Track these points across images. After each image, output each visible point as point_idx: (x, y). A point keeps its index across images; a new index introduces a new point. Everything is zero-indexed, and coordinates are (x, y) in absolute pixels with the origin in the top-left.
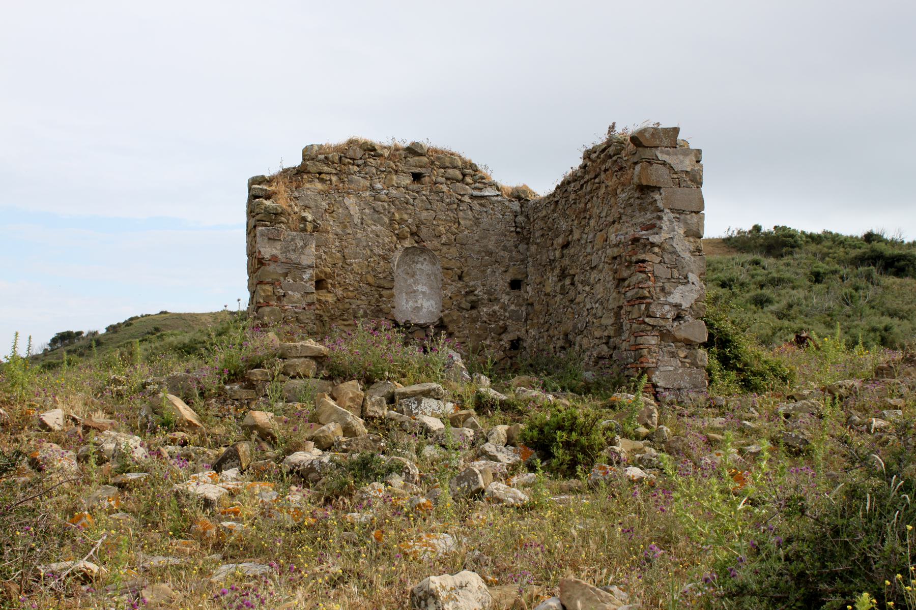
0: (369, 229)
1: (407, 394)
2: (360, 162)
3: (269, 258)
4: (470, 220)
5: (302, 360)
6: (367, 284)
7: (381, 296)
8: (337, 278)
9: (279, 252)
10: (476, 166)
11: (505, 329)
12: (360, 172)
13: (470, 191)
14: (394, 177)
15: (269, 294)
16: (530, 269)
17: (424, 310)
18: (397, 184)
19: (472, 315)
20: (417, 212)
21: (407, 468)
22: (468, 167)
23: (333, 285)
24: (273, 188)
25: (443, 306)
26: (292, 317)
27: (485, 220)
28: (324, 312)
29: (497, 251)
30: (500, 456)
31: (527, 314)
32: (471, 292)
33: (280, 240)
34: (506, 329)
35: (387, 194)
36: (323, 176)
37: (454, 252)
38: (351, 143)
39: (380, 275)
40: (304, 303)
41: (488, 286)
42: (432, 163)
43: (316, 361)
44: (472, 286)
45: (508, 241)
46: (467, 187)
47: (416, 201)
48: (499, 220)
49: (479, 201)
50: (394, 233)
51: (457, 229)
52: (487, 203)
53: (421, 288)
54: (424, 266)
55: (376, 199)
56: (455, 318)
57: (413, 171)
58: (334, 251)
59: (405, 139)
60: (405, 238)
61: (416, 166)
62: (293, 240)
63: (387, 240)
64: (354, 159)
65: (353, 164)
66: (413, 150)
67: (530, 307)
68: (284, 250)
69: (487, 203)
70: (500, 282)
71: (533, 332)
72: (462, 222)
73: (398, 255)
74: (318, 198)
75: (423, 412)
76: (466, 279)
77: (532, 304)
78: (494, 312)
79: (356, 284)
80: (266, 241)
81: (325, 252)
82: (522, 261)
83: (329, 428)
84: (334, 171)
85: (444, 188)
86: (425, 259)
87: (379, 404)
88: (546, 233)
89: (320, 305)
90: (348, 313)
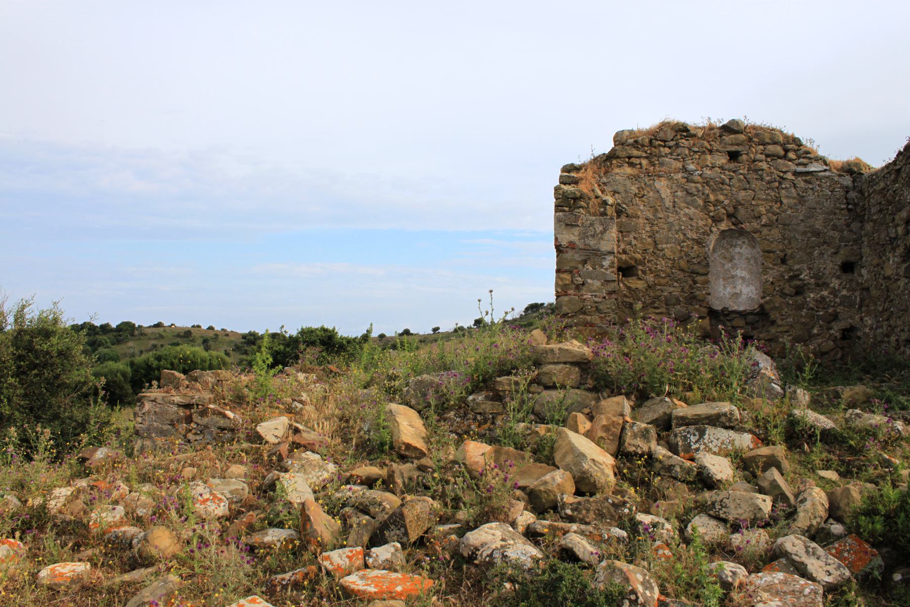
0: (682, 212)
1: (687, 418)
2: (672, 143)
3: (567, 245)
4: (794, 198)
5: (561, 366)
6: (680, 270)
7: (695, 282)
8: (648, 265)
9: (577, 238)
10: (799, 140)
11: (835, 317)
12: (671, 154)
13: (793, 167)
14: (709, 157)
15: (567, 282)
16: (866, 250)
17: (744, 297)
18: (712, 164)
19: (796, 301)
20: (734, 192)
21: (633, 592)
22: (791, 142)
23: (644, 272)
24: (580, 175)
25: (763, 292)
26: (592, 307)
27: (811, 197)
28: (634, 299)
29: (826, 231)
30: (814, 565)
31: (862, 300)
32: (795, 277)
33: (578, 226)
34: (837, 316)
35: (701, 175)
36: (633, 160)
37: (775, 233)
38: (664, 126)
39: (694, 260)
40: (604, 291)
41: (815, 270)
42: (750, 140)
43: (580, 367)
44: (797, 270)
45: (839, 219)
46: (790, 163)
47: (732, 181)
48: (828, 197)
49: (804, 178)
50: (708, 215)
51: (779, 208)
52: (813, 180)
53: (739, 273)
54: (743, 250)
55: (689, 180)
56: (777, 305)
57: (728, 149)
58: (644, 237)
59: (721, 118)
60: (721, 220)
61: (732, 145)
62: (592, 225)
63: (701, 223)
64: (665, 141)
65: (665, 146)
66: (730, 129)
67: (865, 293)
68: (582, 236)
69: (813, 180)
70: (829, 265)
71: (869, 321)
72: (785, 201)
73: (712, 240)
74: (628, 182)
75: (706, 446)
76: (790, 262)
77: (867, 289)
78: (823, 298)
79: (668, 270)
80: (563, 227)
81: (635, 238)
82: (855, 241)
83: (553, 479)
84: (644, 155)
85: (764, 165)
86: (744, 242)
87: (645, 435)
88: (885, 207)
89: (630, 293)
90: (659, 300)
